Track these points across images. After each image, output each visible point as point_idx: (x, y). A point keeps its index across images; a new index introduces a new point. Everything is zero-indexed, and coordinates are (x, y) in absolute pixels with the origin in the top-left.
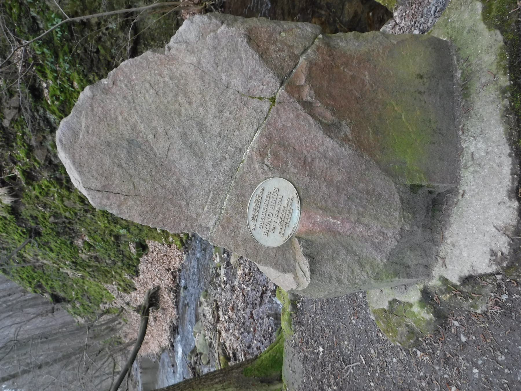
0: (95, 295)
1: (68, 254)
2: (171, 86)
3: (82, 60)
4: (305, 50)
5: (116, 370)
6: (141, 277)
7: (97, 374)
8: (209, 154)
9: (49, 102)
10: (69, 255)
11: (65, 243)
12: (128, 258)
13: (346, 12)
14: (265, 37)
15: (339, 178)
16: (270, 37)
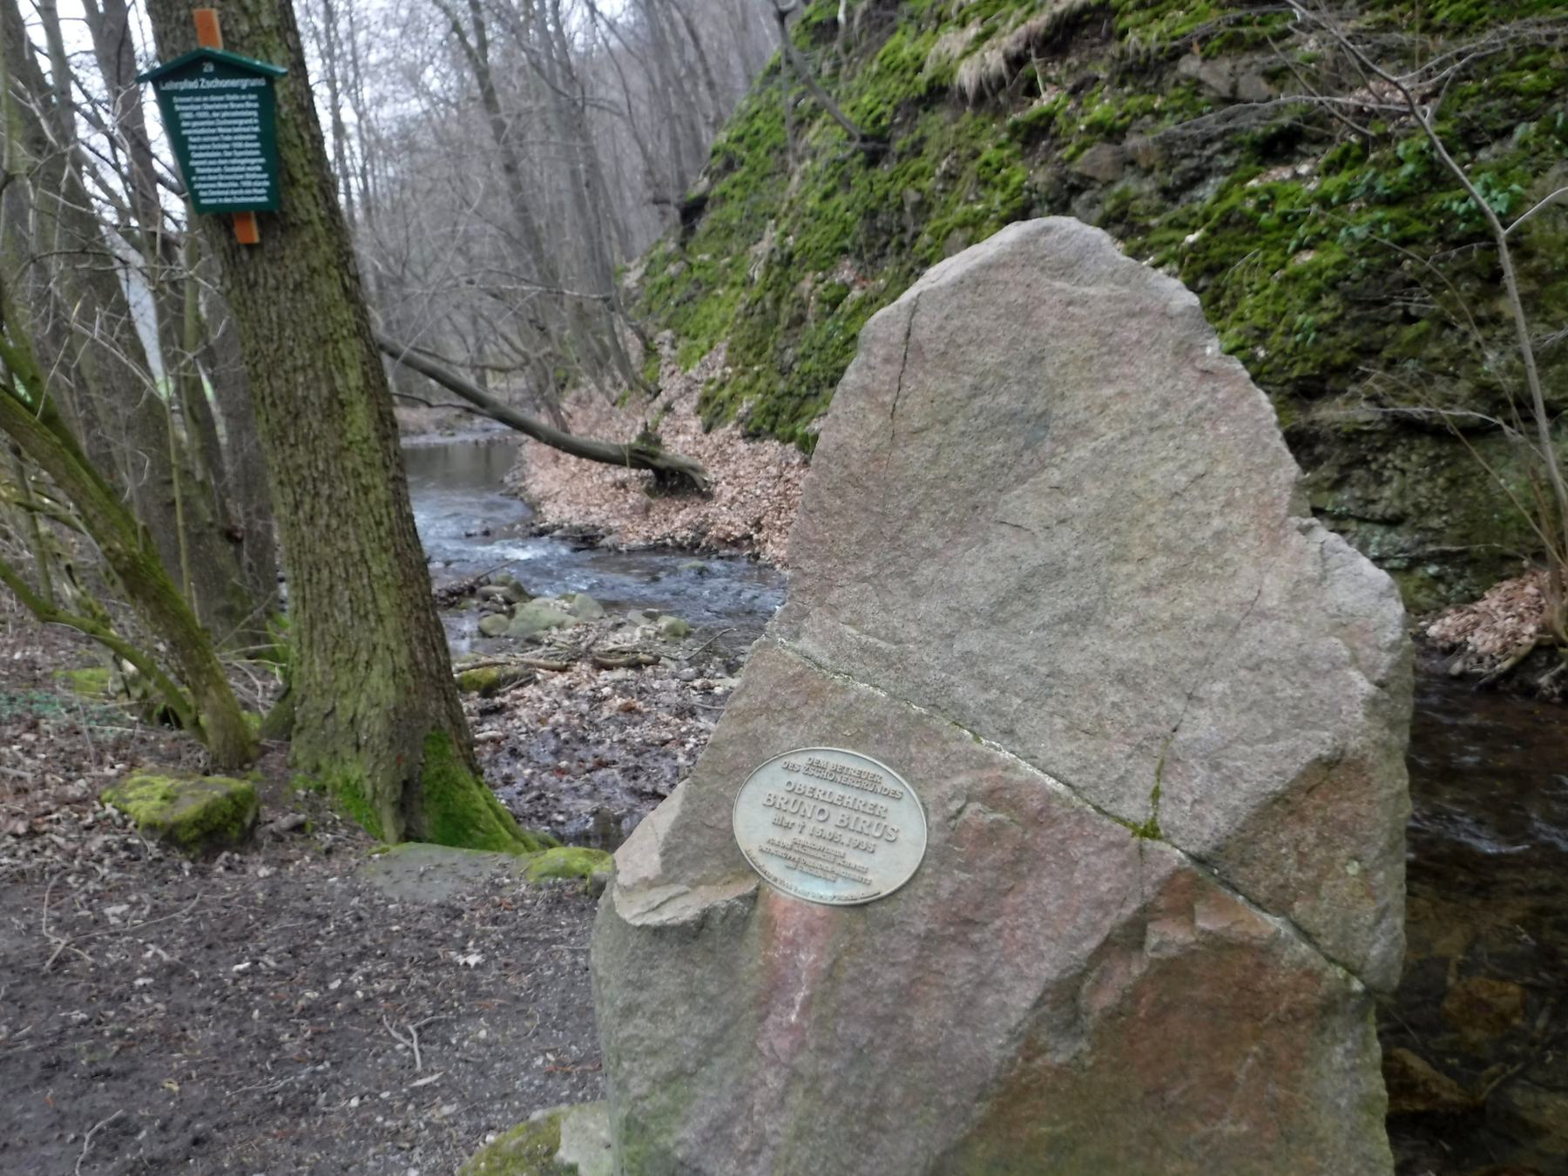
0: (698, 318)
1: (812, 240)
2: (1199, 535)
3: (1381, 274)
4: (1307, 935)
5: (489, 375)
6: (742, 446)
7: (481, 322)
8: (1002, 643)
9: (1254, 183)
10: (812, 244)
11: (845, 233)
12: (796, 409)
13: (1544, 1098)
14: (1341, 812)
15: (919, 1025)
16: (1342, 827)
